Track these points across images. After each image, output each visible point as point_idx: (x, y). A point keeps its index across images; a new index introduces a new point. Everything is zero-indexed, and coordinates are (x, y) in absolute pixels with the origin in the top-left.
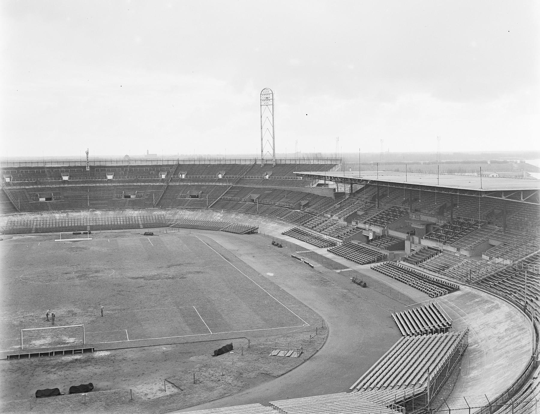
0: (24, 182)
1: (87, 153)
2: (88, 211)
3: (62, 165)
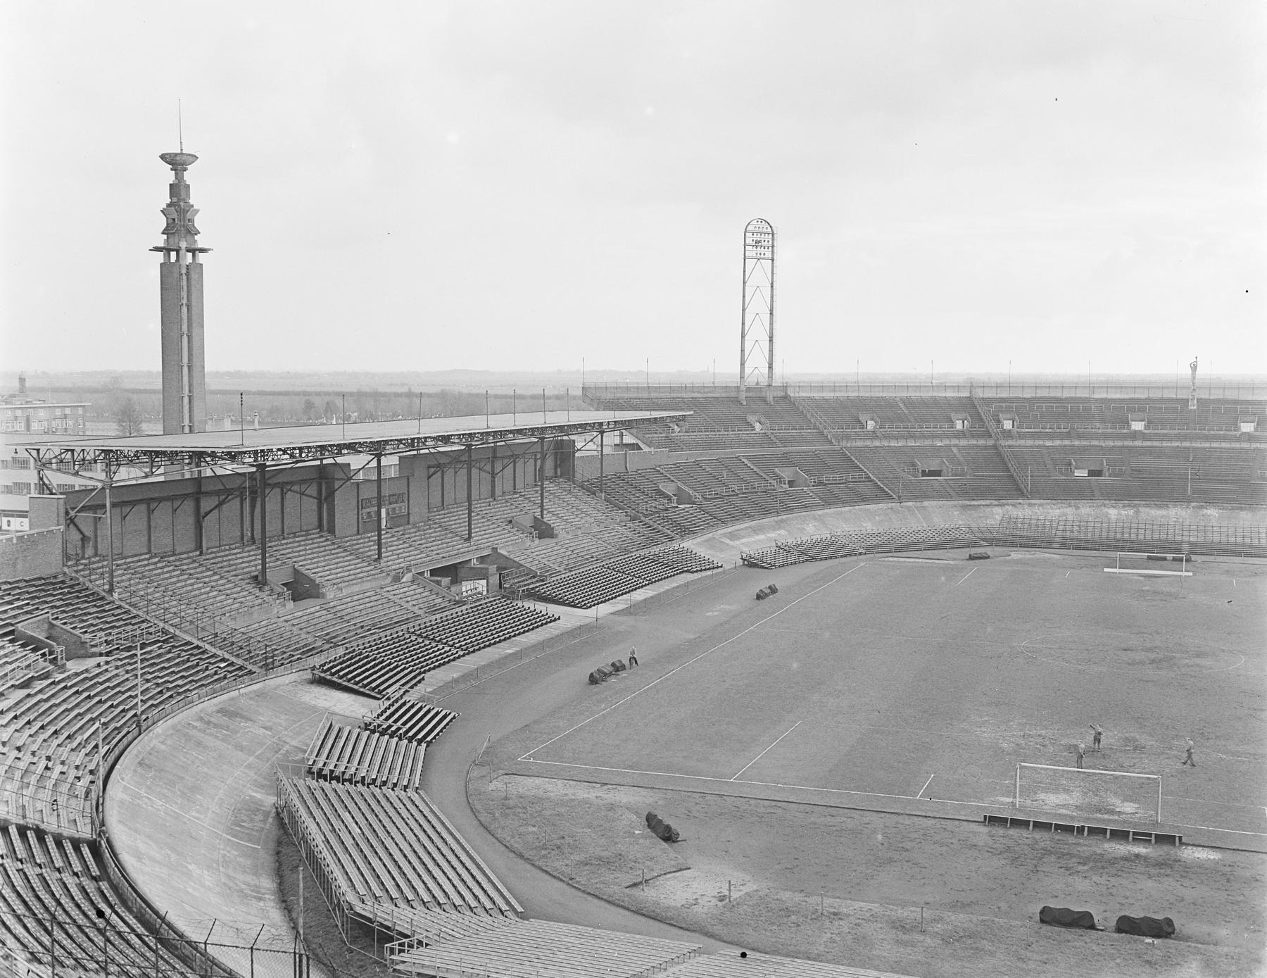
0: (1042, 430)
1: (1194, 368)
2: (1187, 507)
3: (1132, 396)
